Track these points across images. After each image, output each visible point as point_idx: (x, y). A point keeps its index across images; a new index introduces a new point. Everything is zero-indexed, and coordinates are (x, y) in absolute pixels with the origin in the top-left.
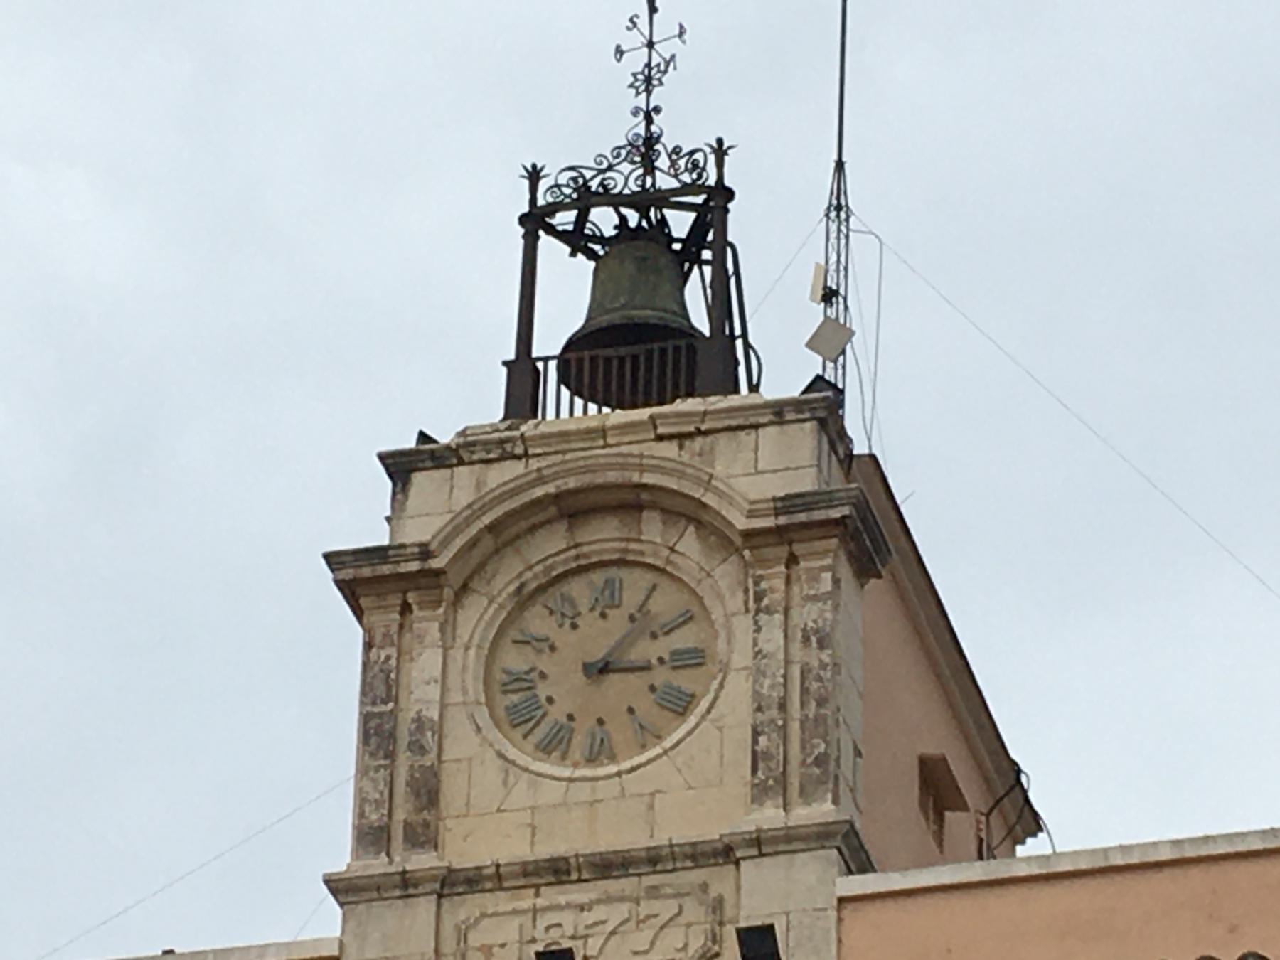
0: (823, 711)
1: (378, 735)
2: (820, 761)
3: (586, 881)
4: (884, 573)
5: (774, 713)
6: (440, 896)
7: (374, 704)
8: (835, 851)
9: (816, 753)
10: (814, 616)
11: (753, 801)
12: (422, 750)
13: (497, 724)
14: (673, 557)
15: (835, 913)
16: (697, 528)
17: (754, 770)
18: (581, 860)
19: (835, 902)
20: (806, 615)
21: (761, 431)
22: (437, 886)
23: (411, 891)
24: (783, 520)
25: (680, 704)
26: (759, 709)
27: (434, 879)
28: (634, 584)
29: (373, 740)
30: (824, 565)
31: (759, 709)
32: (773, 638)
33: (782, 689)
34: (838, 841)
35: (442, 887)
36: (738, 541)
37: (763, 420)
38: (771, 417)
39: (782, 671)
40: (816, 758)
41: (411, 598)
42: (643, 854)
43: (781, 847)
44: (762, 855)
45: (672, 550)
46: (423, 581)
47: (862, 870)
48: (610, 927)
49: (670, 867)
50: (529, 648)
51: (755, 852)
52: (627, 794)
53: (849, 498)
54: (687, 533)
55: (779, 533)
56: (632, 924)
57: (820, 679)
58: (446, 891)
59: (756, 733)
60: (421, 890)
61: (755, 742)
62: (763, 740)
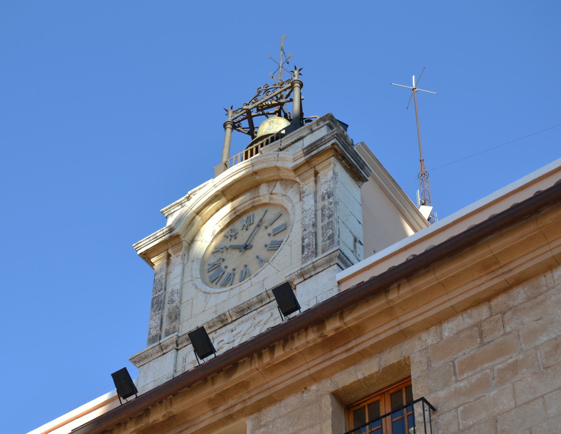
0: (330, 220)
1: (158, 304)
2: (331, 237)
3: (235, 320)
4: (368, 178)
5: (311, 229)
6: (177, 350)
7: (156, 293)
8: (336, 265)
9: (328, 235)
10: (325, 189)
11: (409, 357)
12: (173, 301)
13: (207, 285)
14: (273, 196)
15: (337, 288)
16: (281, 184)
17: (303, 252)
18: (230, 312)
19: (337, 284)
20: (323, 189)
21: (304, 139)
22: (175, 345)
23: (165, 351)
24: (307, 156)
25: (275, 247)
26: (305, 230)
27: (172, 343)
28: (258, 214)
29: (155, 306)
30: (332, 172)
31: (305, 230)
32: (309, 202)
33: (314, 219)
34: (337, 261)
35: (177, 346)
36: (292, 175)
37: (304, 134)
38: (308, 131)
39: (314, 213)
40: (328, 237)
41: (170, 251)
42: (255, 300)
43: (313, 273)
44: (305, 280)
45: (271, 194)
46: (173, 242)
47: (347, 266)
48: (242, 333)
49: (268, 300)
50: (219, 253)
51: (302, 279)
52: (253, 284)
53: (333, 136)
54: (276, 187)
55: (307, 162)
56: (253, 328)
57: (329, 209)
58: (179, 347)
59: (303, 239)
60: (168, 349)
61: (303, 242)
62: (306, 241)
